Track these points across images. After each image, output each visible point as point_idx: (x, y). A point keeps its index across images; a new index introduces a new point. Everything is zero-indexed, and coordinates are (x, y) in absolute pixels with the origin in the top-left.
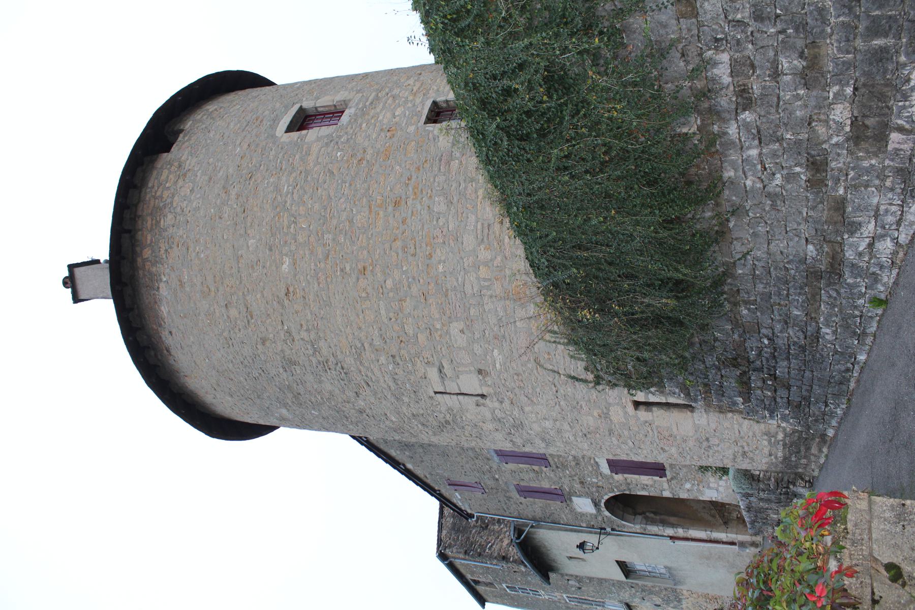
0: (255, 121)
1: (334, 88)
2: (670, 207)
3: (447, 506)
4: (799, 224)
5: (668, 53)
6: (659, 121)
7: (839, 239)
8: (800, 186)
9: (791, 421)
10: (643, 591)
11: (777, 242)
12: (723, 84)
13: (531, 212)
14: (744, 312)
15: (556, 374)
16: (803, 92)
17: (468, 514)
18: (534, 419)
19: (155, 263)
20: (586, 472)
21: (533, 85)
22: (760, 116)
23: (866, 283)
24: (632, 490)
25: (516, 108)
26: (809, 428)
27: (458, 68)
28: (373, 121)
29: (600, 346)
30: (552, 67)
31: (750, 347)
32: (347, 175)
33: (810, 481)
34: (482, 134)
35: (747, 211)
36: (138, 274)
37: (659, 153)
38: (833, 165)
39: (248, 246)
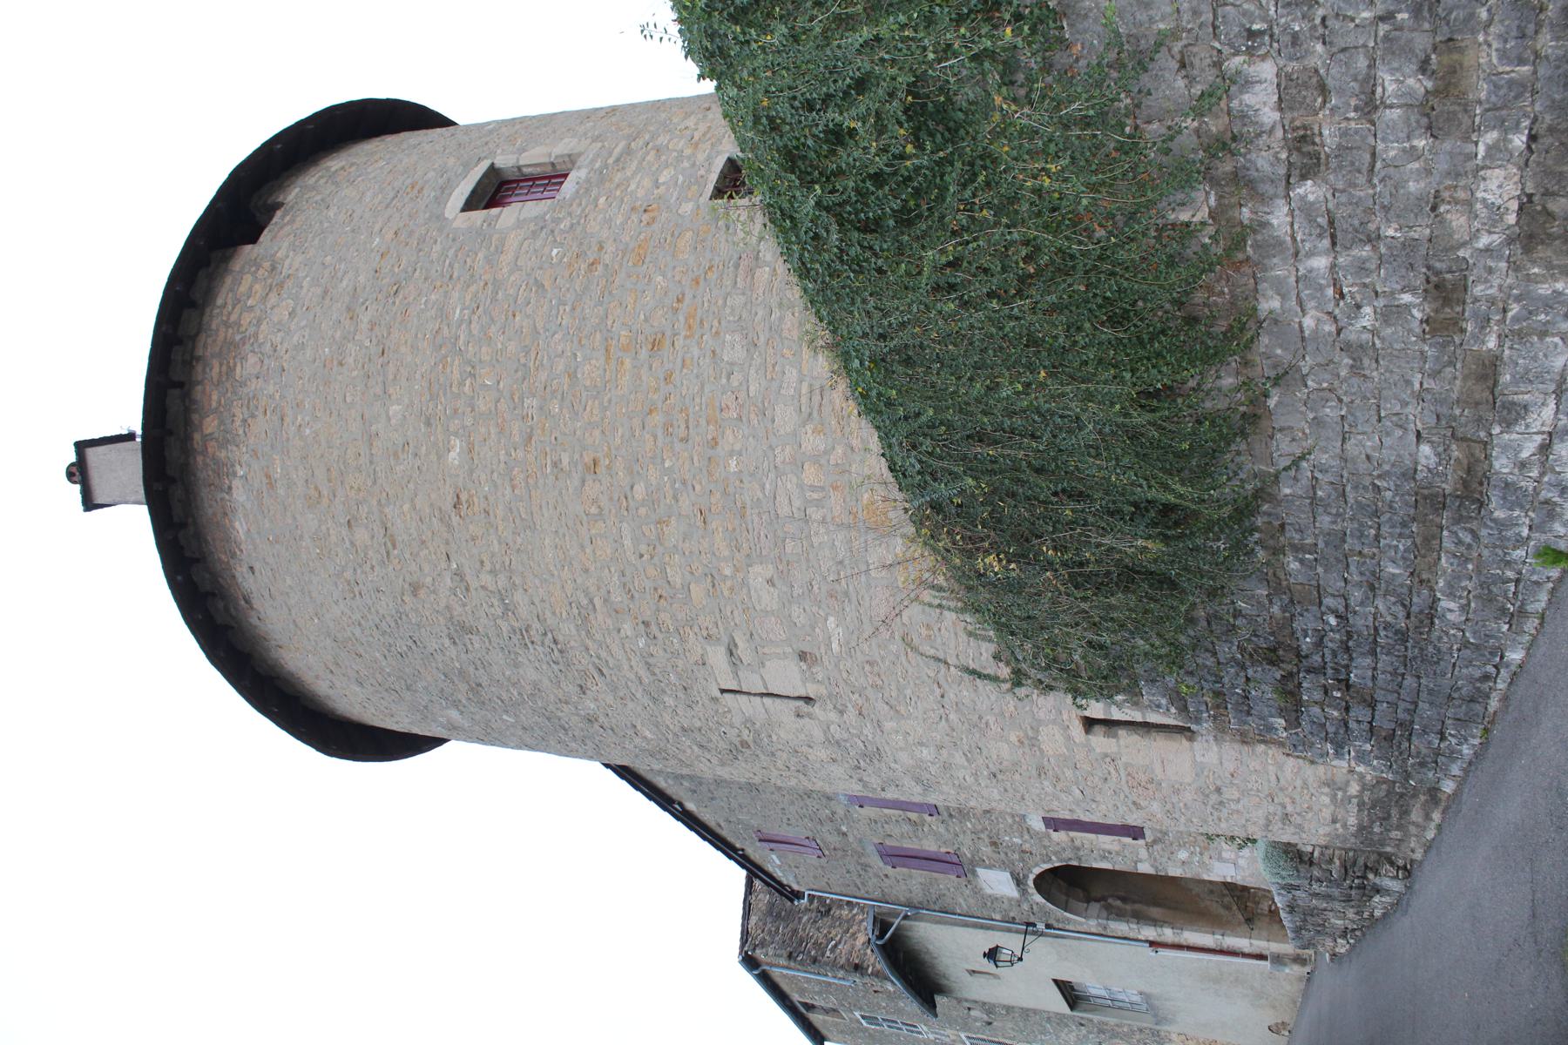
0: (409, 190)
1: (554, 132)
2: (1154, 367)
3: (758, 877)
4: (1405, 404)
5: (1152, 59)
6: (1134, 198)
7: (1482, 434)
8: (1410, 331)
9: (1375, 762)
10: (1101, 1031)
11: (1360, 437)
12: (1262, 125)
13: (886, 370)
14: (1292, 566)
15: (942, 665)
16: (1424, 142)
17: (792, 892)
18: (902, 744)
19: (224, 444)
20: (1002, 826)
21: (886, 122)
22: (1335, 190)
23: (1531, 520)
24: (1083, 859)
25: (854, 167)
26: (1408, 776)
27: (740, 88)
28: (618, 193)
29: (1021, 619)
30: (923, 87)
31: (1303, 630)
32: (568, 290)
33: (1405, 868)
34: (792, 218)
35: (1304, 378)
36: (195, 461)
37: (1133, 260)
38: (1478, 290)
39: (388, 416)
